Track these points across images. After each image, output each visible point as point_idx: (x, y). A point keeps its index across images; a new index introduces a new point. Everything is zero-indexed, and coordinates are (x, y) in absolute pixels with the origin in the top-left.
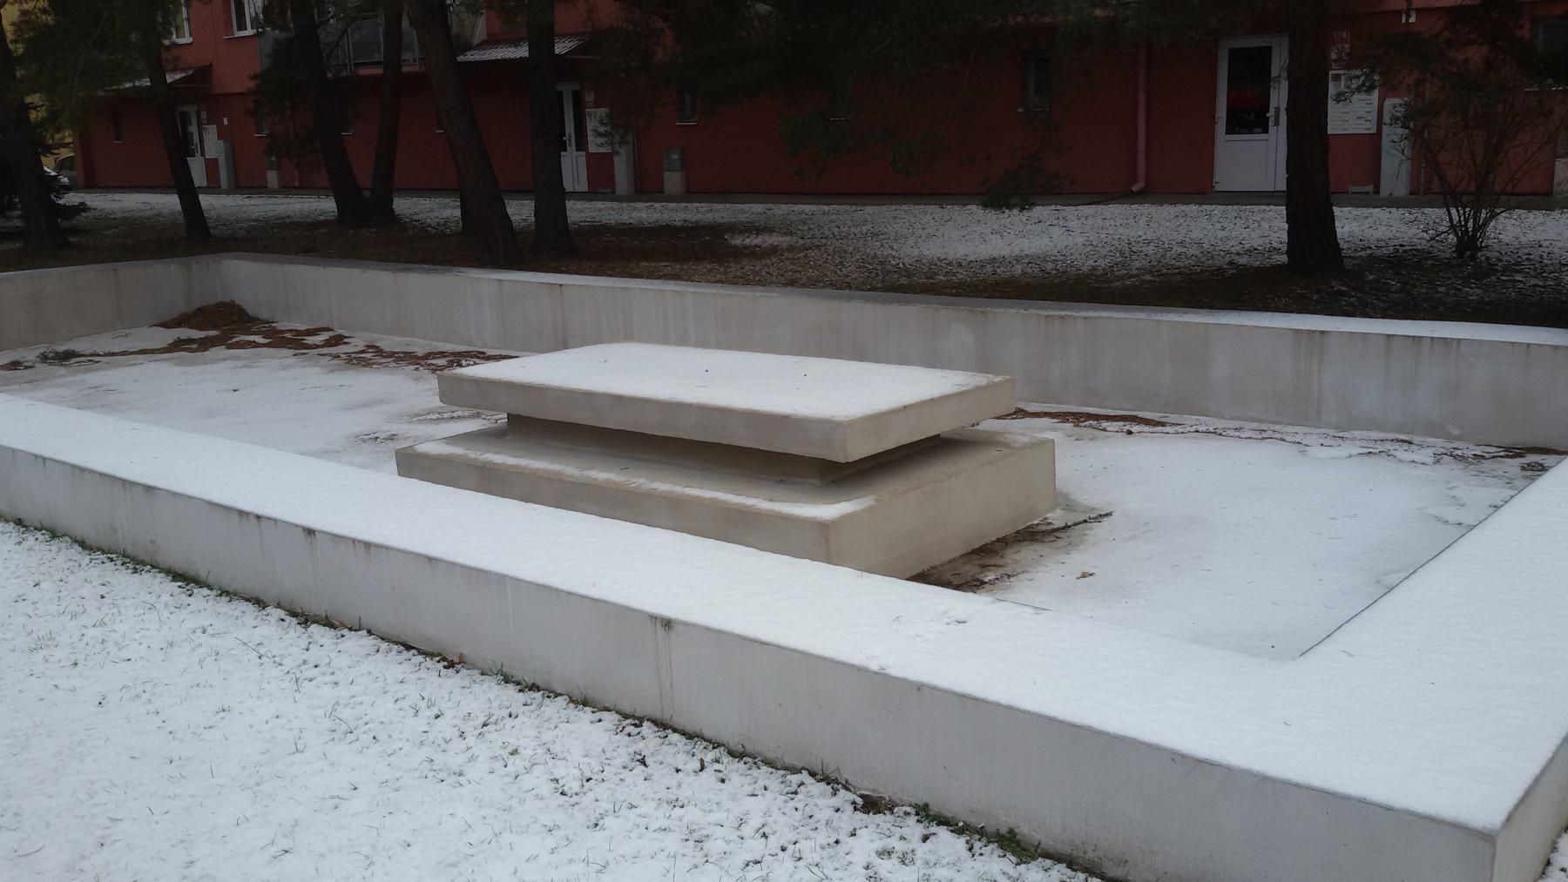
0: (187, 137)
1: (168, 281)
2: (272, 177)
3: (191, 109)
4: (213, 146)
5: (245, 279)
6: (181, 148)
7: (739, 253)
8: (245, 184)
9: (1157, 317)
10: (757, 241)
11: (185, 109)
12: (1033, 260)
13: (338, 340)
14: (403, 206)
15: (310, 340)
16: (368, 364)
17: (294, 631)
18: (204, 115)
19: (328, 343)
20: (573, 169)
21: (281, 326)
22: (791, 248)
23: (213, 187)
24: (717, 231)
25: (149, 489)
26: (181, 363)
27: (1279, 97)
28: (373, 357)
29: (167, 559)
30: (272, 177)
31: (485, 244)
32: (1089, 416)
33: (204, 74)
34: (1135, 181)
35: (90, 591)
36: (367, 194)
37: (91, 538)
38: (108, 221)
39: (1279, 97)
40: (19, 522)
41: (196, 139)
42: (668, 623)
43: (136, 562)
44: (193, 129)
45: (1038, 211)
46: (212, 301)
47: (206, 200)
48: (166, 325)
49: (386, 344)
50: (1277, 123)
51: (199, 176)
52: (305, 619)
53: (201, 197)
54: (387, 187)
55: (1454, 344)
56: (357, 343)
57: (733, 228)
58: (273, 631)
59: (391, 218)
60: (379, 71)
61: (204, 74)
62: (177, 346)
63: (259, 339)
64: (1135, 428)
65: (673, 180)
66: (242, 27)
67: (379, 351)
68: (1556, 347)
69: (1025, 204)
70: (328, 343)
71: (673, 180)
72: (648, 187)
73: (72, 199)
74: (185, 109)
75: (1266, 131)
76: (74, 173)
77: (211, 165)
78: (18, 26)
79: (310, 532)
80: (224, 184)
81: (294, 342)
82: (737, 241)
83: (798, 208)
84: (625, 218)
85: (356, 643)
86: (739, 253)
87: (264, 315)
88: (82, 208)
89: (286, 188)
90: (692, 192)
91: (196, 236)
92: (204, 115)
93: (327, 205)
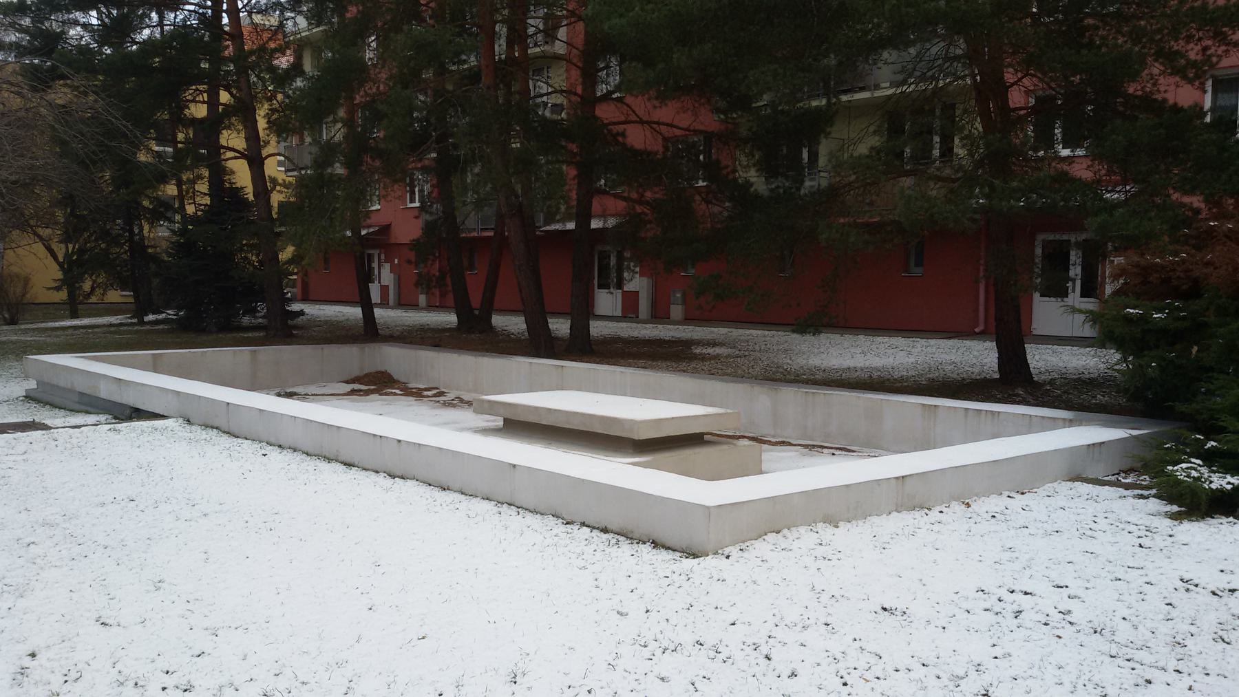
0: (371, 269)
1: (353, 357)
2: (422, 299)
3: (375, 252)
4: (386, 276)
5: (394, 358)
6: (366, 277)
7: (695, 357)
8: (405, 303)
9: (861, 395)
10: (710, 351)
11: (371, 252)
12: (870, 369)
13: (442, 394)
14: (498, 321)
15: (426, 393)
16: (454, 406)
17: (390, 481)
18: (383, 257)
19: (435, 396)
20: (607, 302)
21: (410, 386)
22: (729, 356)
23: (384, 304)
24: (688, 343)
25: (339, 427)
26: (353, 401)
27: (1075, 271)
28: (460, 402)
29: (341, 458)
30: (422, 299)
31: (540, 345)
32: (814, 446)
33: (386, 229)
34: (977, 326)
35: (311, 468)
36: (477, 312)
37: (310, 451)
38: (316, 323)
39: (1075, 271)
40: (280, 446)
41: (376, 272)
42: (514, 466)
43: (329, 460)
44: (375, 265)
45: (823, 336)
46: (372, 370)
47: (378, 312)
48: (347, 382)
49: (466, 398)
50: (1074, 291)
51: (375, 296)
52: (393, 477)
53: (376, 310)
54: (489, 307)
55: (1001, 416)
56: (450, 396)
57: (699, 343)
58: (382, 480)
59: (490, 328)
60: (491, 234)
61: (386, 229)
62: (352, 392)
63: (398, 392)
64: (837, 452)
65: (677, 311)
66: (412, 201)
67: (461, 400)
68: (1054, 419)
69: (817, 332)
70: (435, 396)
71: (677, 311)
72: (659, 314)
73: (296, 307)
74: (371, 252)
75: (1082, 296)
76: (294, 290)
77: (384, 289)
78: (281, 204)
79: (399, 441)
80: (391, 302)
81: (417, 394)
82: (698, 350)
83: (748, 332)
84: (636, 334)
85: (410, 483)
86: (695, 357)
87: (402, 379)
88: (302, 313)
89: (430, 307)
90: (688, 319)
91: (370, 332)
92: (383, 257)
93: (451, 319)
